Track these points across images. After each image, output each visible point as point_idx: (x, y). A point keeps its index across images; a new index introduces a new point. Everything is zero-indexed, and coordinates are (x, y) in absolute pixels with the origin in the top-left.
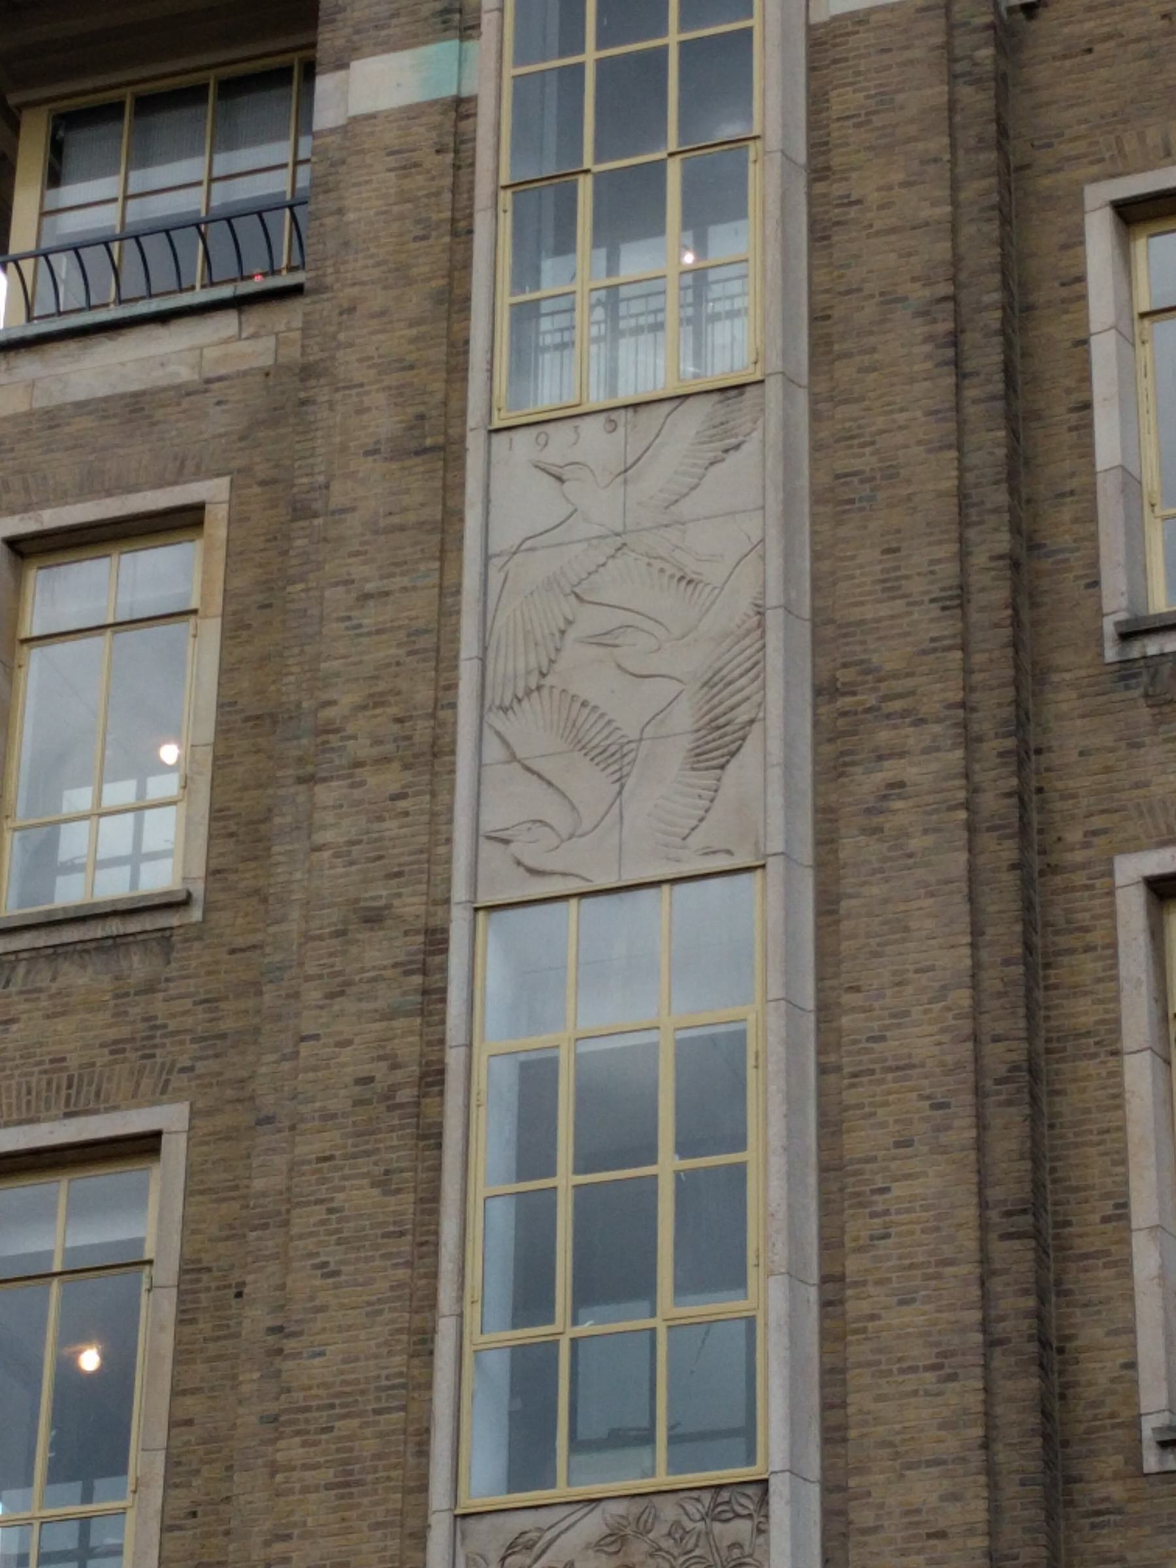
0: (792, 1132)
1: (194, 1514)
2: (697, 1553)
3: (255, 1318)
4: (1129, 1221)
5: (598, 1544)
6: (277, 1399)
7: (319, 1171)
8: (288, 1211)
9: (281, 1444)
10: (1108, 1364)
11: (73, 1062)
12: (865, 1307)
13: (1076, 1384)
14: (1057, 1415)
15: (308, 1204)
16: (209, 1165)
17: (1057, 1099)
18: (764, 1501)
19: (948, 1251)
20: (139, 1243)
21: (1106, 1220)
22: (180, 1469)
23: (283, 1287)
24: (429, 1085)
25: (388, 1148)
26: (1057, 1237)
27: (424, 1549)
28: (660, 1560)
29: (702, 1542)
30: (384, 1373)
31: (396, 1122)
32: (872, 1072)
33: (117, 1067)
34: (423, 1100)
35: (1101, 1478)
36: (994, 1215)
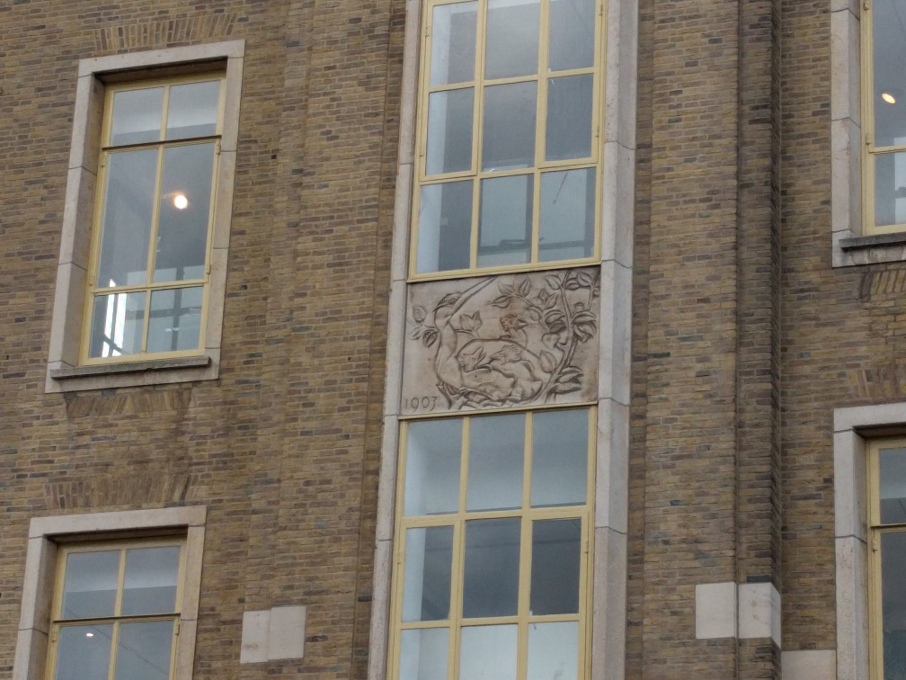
0: (622, 56)
1: (245, 287)
2: (555, 308)
3: (286, 164)
4: (830, 115)
5: (494, 302)
6: (298, 213)
7: (327, 75)
8: (306, 100)
9: (300, 239)
10: (813, 202)
11: (173, 13)
12: (664, 163)
13: (793, 213)
14: (780, 231)
15: (319, 95)
16: (256, 78)
17: (787, 39)
18: (597, 278)
19: (717, 130)
20: (212, 126)
21: (815, 114)
22: (237, 260)
23: (302, 146)
24: (395, 24)
25: (368, 62)
26: (784, 124)
27: (388, 304)
28: (532, 312)
29: (559, 301)
30: (364, 198)
31: (374, 46)
32: (673, 20)
33: (200, 18)
34: (392, 34)
35: (806, 270)
36: (746, 108)
